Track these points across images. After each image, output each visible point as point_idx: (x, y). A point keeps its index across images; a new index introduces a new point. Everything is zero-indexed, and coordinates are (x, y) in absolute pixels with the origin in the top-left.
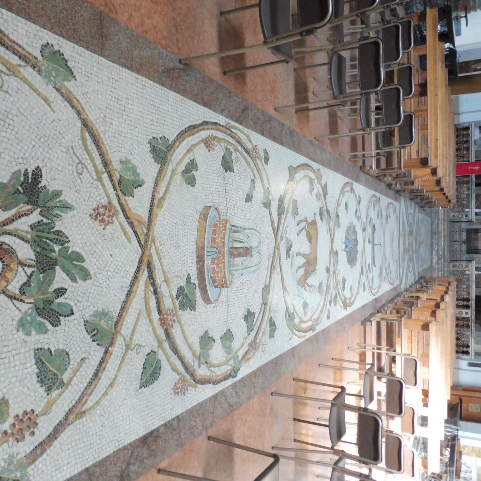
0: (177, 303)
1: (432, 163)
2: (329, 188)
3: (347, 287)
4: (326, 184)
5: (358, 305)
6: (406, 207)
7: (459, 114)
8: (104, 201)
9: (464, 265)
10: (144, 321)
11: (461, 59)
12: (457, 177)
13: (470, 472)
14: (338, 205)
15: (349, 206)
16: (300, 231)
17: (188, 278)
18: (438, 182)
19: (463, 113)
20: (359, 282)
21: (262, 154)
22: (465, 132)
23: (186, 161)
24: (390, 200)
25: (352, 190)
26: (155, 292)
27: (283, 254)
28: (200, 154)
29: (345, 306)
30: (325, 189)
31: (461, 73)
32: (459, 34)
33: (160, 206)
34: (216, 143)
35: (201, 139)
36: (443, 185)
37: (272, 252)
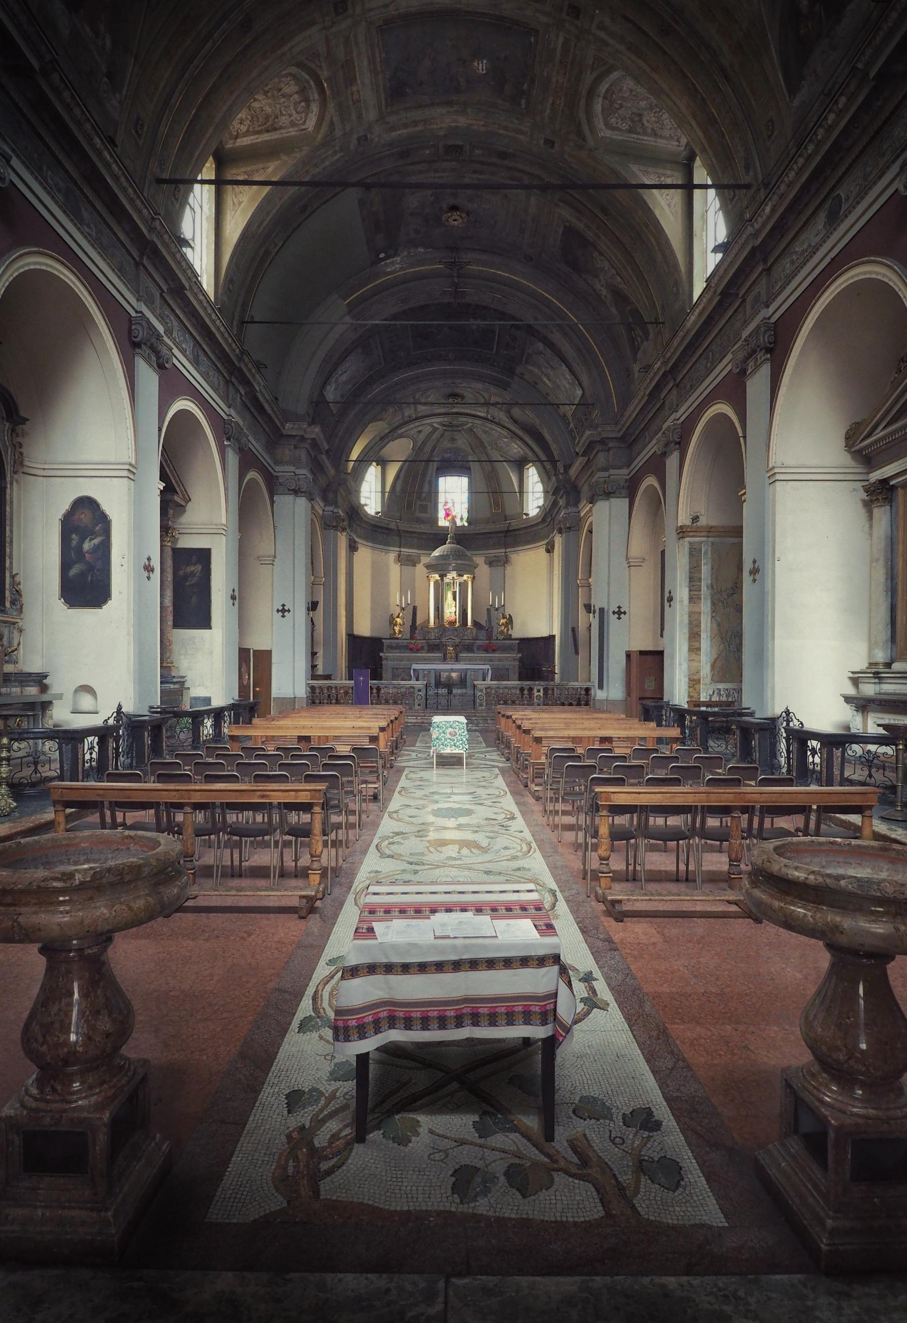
1: (375, 732)
2: (396, 830)
3: (494, 817)
4: (393, 833)
5: (514, 809)
6: (409, 760)
9: (480, 693)
13: (719, 690)
14: (412, 823)
15: (413, 814)
16: (438, 851)
19: (294, 694)
20: (490, 807)
22: (318, 691)
24: (403, 777)
25: (396, 812)
29: (513, 818)
32: (208, 700)
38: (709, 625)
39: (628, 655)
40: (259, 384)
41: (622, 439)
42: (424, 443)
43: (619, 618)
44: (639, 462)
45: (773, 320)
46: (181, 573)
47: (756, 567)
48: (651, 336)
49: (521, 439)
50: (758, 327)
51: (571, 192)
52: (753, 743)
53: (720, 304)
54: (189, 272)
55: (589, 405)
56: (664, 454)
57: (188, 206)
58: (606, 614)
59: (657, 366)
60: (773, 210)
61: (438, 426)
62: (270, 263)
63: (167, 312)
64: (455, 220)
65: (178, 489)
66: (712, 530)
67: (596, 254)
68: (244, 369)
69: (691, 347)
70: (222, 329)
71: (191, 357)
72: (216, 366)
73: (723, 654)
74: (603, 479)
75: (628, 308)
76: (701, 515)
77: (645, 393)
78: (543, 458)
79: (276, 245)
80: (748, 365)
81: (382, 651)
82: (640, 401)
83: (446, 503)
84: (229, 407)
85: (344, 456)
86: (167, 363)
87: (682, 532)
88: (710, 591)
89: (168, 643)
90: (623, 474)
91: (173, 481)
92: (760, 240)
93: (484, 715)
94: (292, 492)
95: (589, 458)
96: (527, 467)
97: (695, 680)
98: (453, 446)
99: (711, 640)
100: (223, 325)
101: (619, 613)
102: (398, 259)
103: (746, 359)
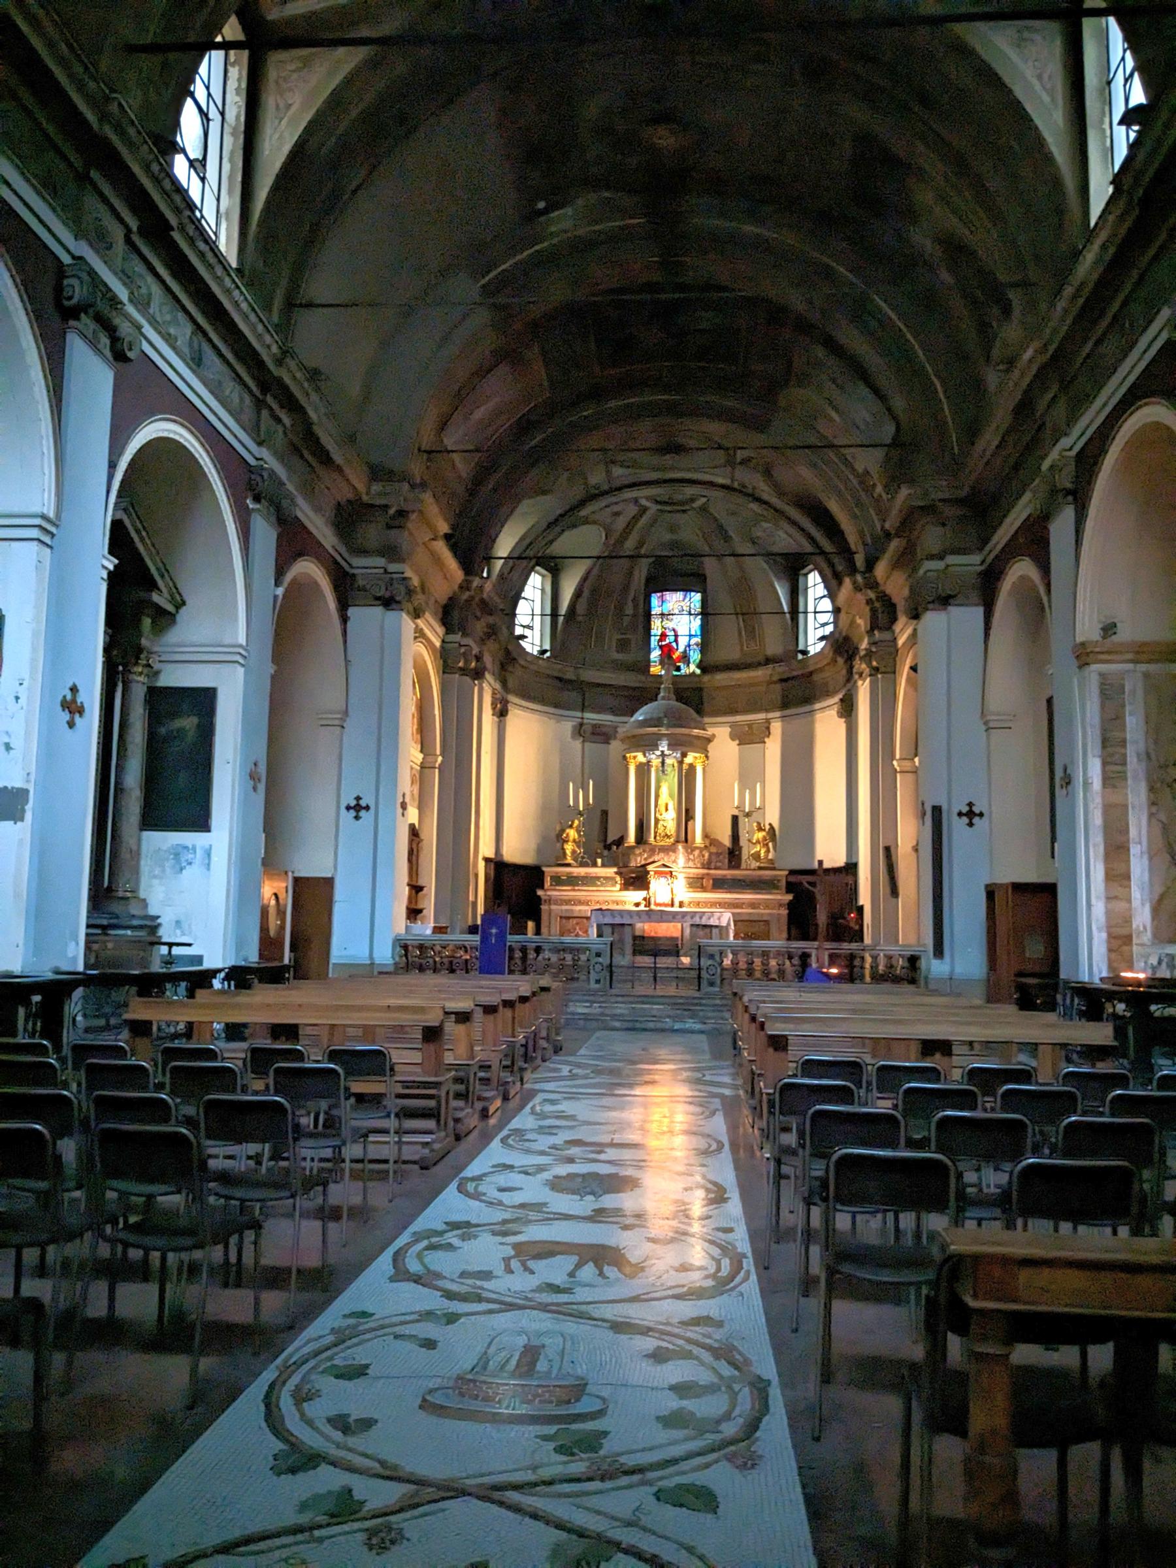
0: (583, 1455)
1: (433, 1019)
6: (555, 1079)
7: (372, 964)
8: (361, 1537)
10: (594, 1502)
11: (252, 956)
12: (511, 972)
14: (500, 1203)
17: (546, 1438)
18: (490, 1010)
21: (352, 1321)
23: (328, 1429)
25: (478, 1178)
26: (550, 1483)
27: (563, 1298)
28: (318, 1410)
30: (454, 1226)
31: (282, 958)
32: (199, 959)
33: (395, 1467)
34: (308, 1386)
35: (293, 1408)
36: (494, 1000)
37: (550, 1315)
44: (1002, 536)
46: (163, 730)
49: (794, 523)
54: (177, 198)
58: (944, 815)
61: (648, 504)
63: (140, 268)
68: (287, 380)
70: (244, 306)
71: (186, 350)
78: (828, 546)
83: (663, 636)
84: (260, 444)
86: (130, 349)
87: (1083, 655)
88: (1144, 764)
90: (971, 563)
100: (246, 299)
101: (971, 815)
102: (569, 211)
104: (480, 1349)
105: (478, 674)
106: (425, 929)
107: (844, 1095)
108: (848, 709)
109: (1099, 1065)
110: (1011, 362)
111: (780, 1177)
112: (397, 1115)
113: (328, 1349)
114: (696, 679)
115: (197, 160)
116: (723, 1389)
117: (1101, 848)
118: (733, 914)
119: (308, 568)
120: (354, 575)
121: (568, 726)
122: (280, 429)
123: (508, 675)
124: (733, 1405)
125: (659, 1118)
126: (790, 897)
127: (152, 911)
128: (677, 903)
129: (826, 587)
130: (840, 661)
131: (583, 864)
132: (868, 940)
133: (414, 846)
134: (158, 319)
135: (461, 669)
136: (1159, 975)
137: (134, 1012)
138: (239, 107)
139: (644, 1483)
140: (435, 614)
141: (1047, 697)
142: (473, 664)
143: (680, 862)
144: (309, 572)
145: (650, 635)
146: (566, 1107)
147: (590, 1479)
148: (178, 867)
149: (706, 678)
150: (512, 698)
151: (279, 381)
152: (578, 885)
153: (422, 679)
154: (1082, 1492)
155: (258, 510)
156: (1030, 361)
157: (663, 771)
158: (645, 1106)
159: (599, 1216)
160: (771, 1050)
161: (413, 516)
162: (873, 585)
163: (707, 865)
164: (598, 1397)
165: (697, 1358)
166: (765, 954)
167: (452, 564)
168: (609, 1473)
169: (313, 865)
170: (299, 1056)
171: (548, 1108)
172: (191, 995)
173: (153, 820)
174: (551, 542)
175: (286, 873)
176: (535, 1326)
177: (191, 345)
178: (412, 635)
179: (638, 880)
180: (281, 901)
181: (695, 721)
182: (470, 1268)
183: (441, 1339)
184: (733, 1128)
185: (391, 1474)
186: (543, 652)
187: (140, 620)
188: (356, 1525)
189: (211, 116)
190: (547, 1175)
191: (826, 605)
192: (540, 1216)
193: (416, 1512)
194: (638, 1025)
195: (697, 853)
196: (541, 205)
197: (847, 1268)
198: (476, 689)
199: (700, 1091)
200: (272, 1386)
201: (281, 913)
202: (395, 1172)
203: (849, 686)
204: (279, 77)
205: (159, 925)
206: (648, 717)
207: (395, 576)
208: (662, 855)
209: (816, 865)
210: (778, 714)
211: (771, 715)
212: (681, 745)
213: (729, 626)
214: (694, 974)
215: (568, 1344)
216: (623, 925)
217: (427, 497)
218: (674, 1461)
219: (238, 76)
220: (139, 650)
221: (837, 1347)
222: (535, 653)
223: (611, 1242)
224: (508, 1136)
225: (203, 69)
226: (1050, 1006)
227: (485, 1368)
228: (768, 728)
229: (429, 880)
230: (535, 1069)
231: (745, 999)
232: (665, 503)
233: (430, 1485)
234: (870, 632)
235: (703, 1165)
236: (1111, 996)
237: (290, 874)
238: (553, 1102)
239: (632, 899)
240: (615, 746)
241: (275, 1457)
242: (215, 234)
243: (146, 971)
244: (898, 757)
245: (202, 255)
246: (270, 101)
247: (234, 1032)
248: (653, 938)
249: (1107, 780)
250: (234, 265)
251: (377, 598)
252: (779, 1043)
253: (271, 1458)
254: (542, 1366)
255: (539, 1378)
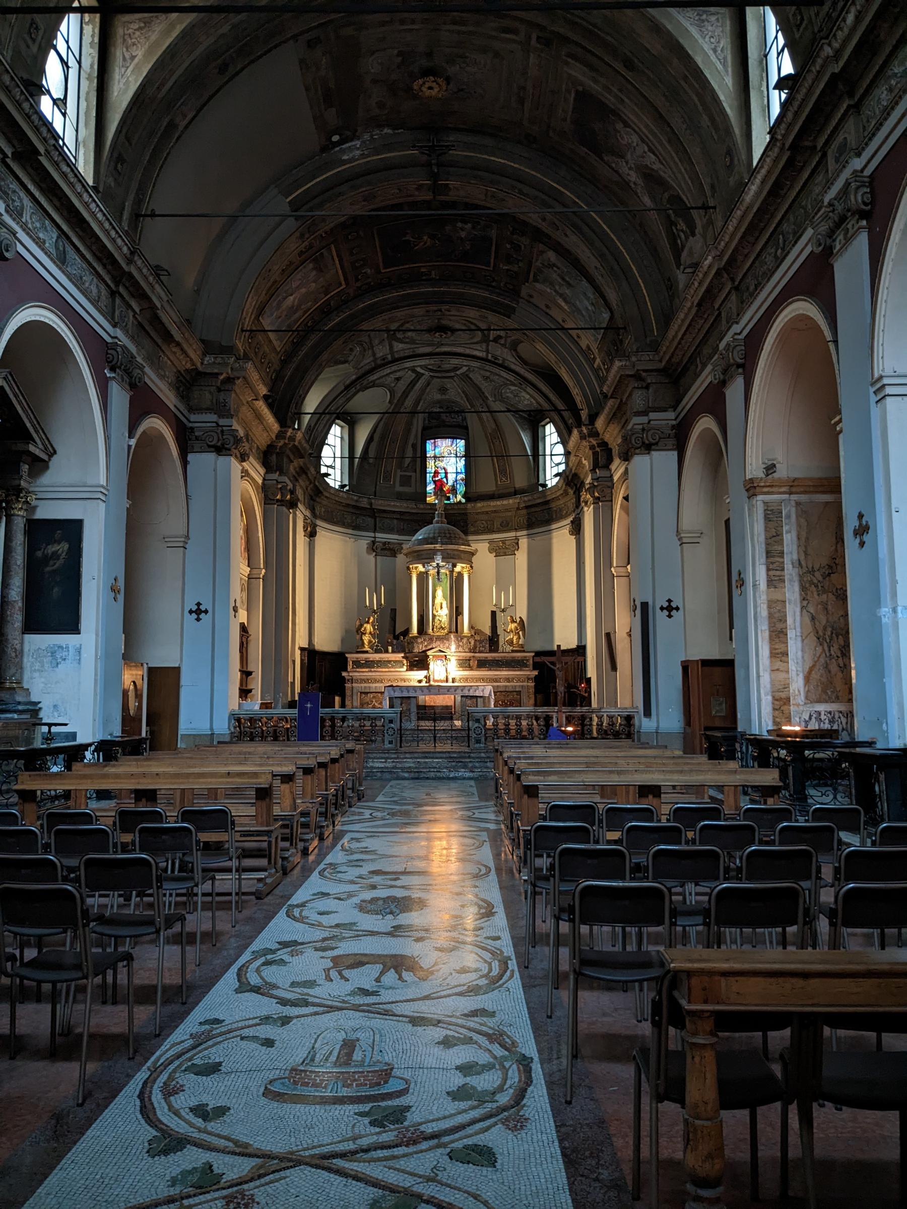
0: (392, 1127)
2: (287, 938)
6: (360, 821)
7: (213, 734)
10: (402, 1164)
11: (116, 731)
12: (323, 738)
13: (819, 713)
14: (320, 925)
16: (342, 977)
17: (361, 1114)
18: (307, 771)
19: (211, 729)
23: (191, 1117)
25: (303, 905)
26: (366, 1151)
28: (181, 1101)
30: (285, 944)
31: (140, 734)
32: (73, 736)
33: (247, 1145)
34: (174, 1083)
35: (163, 1101)
36: (312, 763)
37: (362, 1014)
38: (798, 618)
39: (686, 667)
40: (160, 298)
41: (663, 371)
42: (405, 394)
43: (670, 616)
45: (868, 172)
46: (39, 554)
47: (864, 523)
48: (699, 229)
50: (847, 184)
51: (576, 12)
52: (877, 788)
53: (790, 163)
54: (44, 130)
55: (619, 328)
56: (723, 383)
57: (52, 52)
59: (707, 262)
60: (858, 18)
62: (178, 139)
64: (430, 88)
65: (35, 435)
66: (795, 484)
67: (619, 126)
68: (135, 273)
69: (754, 228)
71: (53, 251)
72: (94, 269)
73: (822, 660)
74: (641, 427)
75: (666, 195)
76: (779, 463)
77: (693, 303)
78: (560, 405)
79: (185, 116)
80: (834, 241)
81: (346, 670)
82: (686, 315)
83: (436, 473)
84: (115, 326)
85: (293, 406)
86: (7, 251)
87: (752, 488)
88: (796, 570)
89: (13, 655)
91: (28, 425)
92: (841, 63)
93: (483, 755)
94: (213, 449)
95: (621, 401)
96: (543, 423)
97: (780, 699)
98: (444, 397)
99: (803, 641)
100: (101, 210)
101: (670, 609)
102: (358, 143)
103: (831, 234)
104: (308, 1045)
105: (293, 505)
106: (254, 705)
107: (582, 834)
108: (577, 528)
109: (770, 801)
110: (696, 265)
111: (535, 893)
112: (238, 857)
113: (188, 1051)
114: (462, 507)
115: (59, 99)
116: (497, 1067)
117: (767, 634)
118: (493, 687)
119: (155, 423)
120: (192, 429)
121: (364, 544)
122: (131, 314)
123: (316, 504)
124: (505, 1080)
125: (439, 845)
126: (536, 673)
127: (34, 698)
128: (450, 680)
129: (559, 435)
130: (571, 492)
131: (377, 651)
132: (594, 704)
133: (244, 640)
134: (30, 226)
135: (278, 500)
136: (810, 728)
137: (22, 783)
138: (93, 57)
139: (438, 1146)
140: (257, 459)
141: (726, 518)
142: (288, 497)
143: (452, 649)
144: (154, 425)
145: (426, 473)
146: (370, 843)
147: (397, 1146)
148: (54, 662)
149: (469, 506)
150: (318, 522)
151: (130, 275)
152: (373, 667)
153: (248, 510)
154: (769, 1132)
155: (114, 378)
156: (710, 266)
157: (439, 579)
158: (429, 840)
159: (396, 931)
160: (526, 796)
161: (238, 382)
162: (594, 434)
163: (473, 650)
164: (402, 1078)
165: (476, 1043)
166: (518, 718)
167: (270, 418)
168: (415, 1138)
169: (163, 657)
170: (157, 816)
171: (355, 845)
172: (68, 768)
173: (32, 626)
174: (349, 400)
175: (142, 665)
176: (351, 1023)
177: (57, 248)
178: (240, 475)
179: (420, 663)
180: (139, 687)
181: (463, 539)
182: (298, 979)
183: (277, 1038)
184: (497, 856)
185: (243, 1151)
186: (343, 486)
187: (19, 466)
188: (217, 1194)
189: (70, 64)
190: (356, 900)
191: (560, 449)
192: (352, 933)
193: (263, 1181)
194: (422, 775)
195: (465, 640)
196: (335, 138)
197: (588, 971)
198: (291, 516)
199: (471, 826)
200: (145, 1083)
201: (138, 696)
202: (237, 902)
203: (578, 511)
204: (124, 34)
205: (40, 709)
206: (426, 536)
207: (224, 428)
208: (438, 643)
209: (555, 648)
210: (525, 532)
211: (519, 534)
212: (452, 558)
213: (486, 467)
214: (464, 734)
215: (377, 1037)
216: (409, 697)
217: (249, 365)
218: (462, 1127)
219: (92, 31)
220: (18, 490)
221: (582, 1027)
222: (337, 487)
223: (407, 952)
224: (324, 870)
225: (63, 27)
226: (731, 756)
227: (313, 1060)
228: (517, 544)
229: (256, 665)
230: (343, 814)
231: (505, 755)
232: (436, 371)
233: (273, 1158)
234: (593, 470)
235: (476, 887)
236: (776, 745)
237: (145, 666)
238: (358, 840)
239: (416, 677)
240: (401, 559)
241: (150, 1142)
242: (75, 158)
243: (31, 747)
244: (615, 565)
245: (64, 175)
246: (118, 53)
247: (103, 795)
248: (433, 707)
249: (771, 583)
250: (91, 183)
251: (209, 446)
252: (532, 791)
253: (146, 1144)
254: (357, 1056)
255: (356, 1066)
